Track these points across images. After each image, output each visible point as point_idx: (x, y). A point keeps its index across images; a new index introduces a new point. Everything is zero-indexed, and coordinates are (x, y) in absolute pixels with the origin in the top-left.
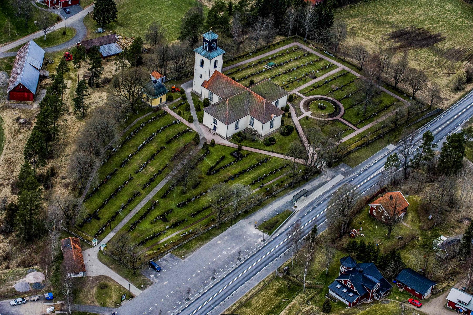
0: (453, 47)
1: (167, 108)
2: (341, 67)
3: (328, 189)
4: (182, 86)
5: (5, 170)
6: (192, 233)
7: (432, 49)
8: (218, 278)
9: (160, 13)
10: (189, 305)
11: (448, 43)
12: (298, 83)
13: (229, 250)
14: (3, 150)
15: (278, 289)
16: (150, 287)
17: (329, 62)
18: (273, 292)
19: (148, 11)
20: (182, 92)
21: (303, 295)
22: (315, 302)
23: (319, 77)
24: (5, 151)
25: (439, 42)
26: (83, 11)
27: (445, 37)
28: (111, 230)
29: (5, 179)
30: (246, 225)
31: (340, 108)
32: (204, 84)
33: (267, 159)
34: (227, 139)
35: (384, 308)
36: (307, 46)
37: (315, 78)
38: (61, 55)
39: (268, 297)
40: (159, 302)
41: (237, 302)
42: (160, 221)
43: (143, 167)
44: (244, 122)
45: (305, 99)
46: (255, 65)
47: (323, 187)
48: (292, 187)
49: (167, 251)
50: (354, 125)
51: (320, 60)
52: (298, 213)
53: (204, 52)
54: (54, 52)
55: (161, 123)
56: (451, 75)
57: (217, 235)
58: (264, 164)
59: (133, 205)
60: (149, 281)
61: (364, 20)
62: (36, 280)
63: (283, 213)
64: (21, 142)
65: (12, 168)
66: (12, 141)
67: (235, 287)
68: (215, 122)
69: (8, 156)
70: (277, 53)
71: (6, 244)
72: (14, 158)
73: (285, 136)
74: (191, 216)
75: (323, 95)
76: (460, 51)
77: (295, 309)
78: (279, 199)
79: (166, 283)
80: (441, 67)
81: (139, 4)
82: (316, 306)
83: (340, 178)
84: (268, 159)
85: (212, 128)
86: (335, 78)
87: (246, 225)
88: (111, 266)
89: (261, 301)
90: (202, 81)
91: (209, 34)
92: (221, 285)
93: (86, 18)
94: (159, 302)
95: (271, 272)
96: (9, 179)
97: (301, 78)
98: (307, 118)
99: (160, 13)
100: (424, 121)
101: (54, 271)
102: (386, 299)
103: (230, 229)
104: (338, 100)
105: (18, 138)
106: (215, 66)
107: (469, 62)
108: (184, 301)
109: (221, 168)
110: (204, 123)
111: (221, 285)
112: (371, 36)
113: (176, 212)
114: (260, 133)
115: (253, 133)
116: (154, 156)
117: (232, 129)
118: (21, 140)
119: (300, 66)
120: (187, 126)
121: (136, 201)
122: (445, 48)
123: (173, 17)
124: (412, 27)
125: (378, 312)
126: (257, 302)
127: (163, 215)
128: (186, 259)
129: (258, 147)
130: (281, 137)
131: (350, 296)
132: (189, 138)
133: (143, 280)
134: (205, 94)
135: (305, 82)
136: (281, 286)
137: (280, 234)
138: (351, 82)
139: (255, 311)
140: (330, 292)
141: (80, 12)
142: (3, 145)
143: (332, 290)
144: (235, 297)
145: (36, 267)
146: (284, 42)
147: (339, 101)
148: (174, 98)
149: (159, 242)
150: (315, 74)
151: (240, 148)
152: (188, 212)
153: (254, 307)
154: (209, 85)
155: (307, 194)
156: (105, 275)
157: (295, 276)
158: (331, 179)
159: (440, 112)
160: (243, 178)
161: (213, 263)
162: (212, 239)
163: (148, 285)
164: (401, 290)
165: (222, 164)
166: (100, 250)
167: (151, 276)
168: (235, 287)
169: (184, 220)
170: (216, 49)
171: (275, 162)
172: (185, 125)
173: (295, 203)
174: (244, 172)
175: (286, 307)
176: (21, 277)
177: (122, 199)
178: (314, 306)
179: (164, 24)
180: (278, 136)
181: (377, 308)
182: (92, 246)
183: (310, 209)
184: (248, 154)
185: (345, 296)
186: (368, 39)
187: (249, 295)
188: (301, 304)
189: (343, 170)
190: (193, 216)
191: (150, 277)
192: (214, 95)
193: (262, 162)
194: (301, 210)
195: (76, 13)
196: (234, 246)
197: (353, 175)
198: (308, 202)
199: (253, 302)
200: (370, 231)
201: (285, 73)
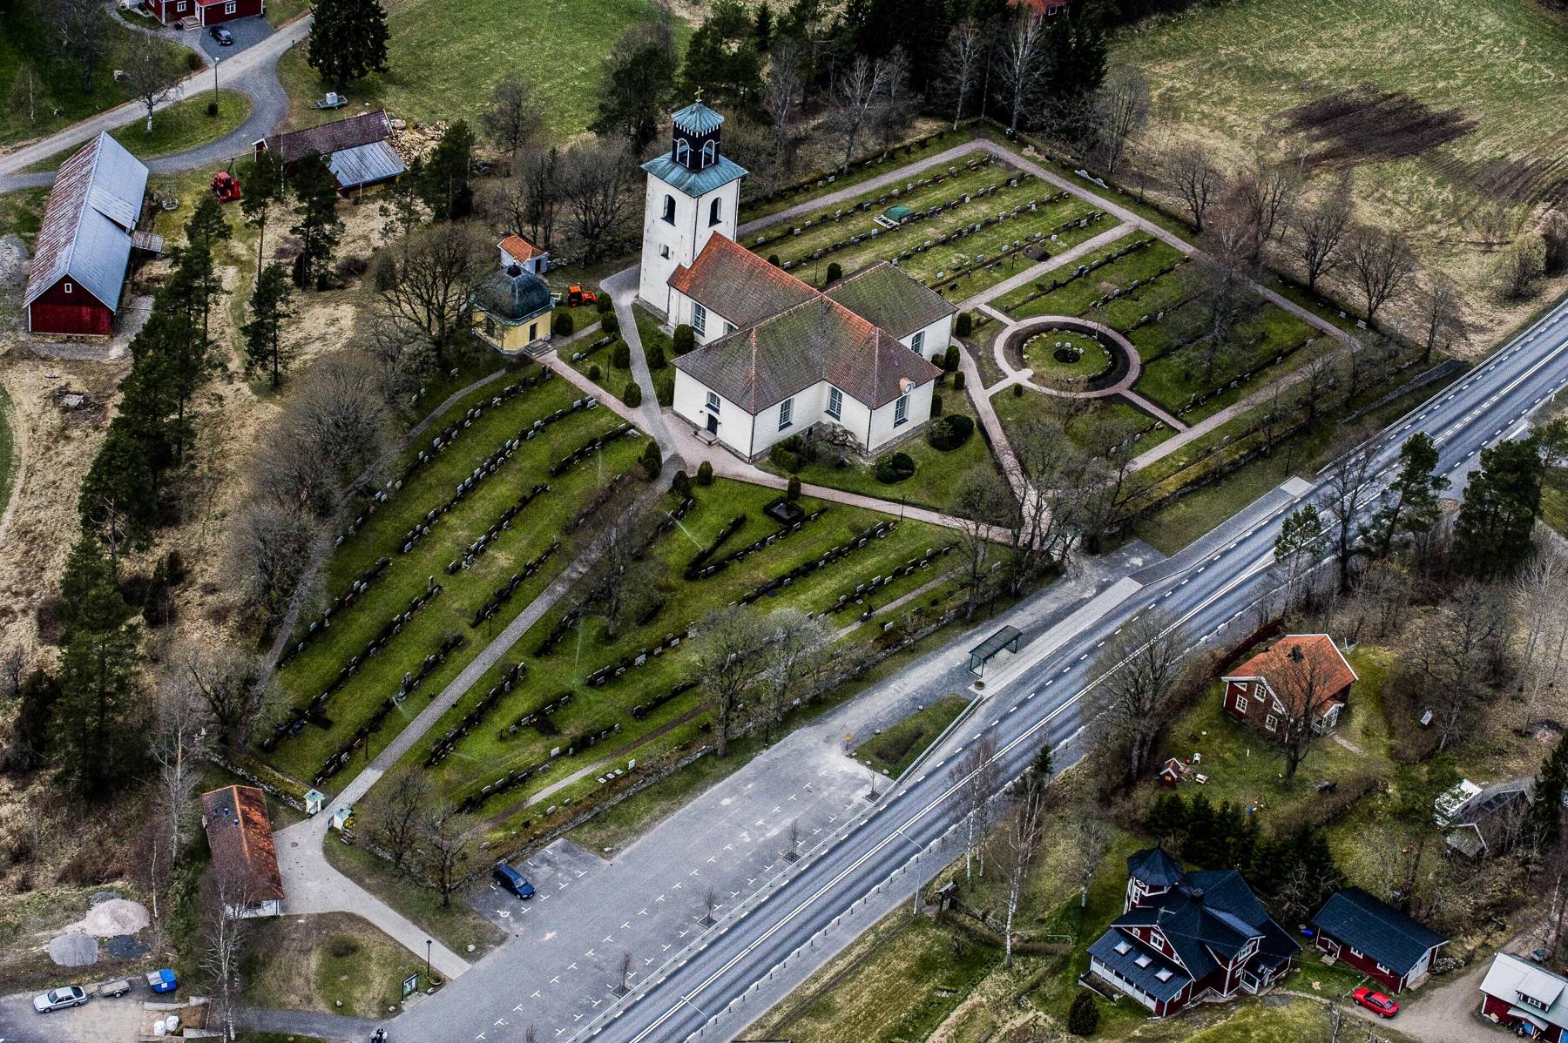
1: (552, 359)
2: (1129, 221)
3: (1086, 626)
5: (17, 564)
6: (635, 770)
8: (723, 921)
10: (627, 1011)
12: (989, 275)
14: (9, 496)
16: (497, 950)
17: (1091, 206)
18: (903, 965)
20: (605, 304)
21: (1005, 976)
22: (1044, 1001)
24: (15, 499)
25: (1456, 140)
26: (275, 37)
27: (1476, 123)
28: (368, 761)
29: (16, 594)
30: (816, 744)
31: (1126, 358)
33: (886, 527)
34: (753, 460)
35: (1275, 1020)
36: (1019, 153)
37: (1044, 257)
38: (202, 181)
39: (890, 983)
41: (787, 1000)
42: (530, 734)
43: (475, 552)
44: (809, 405)
45: (1013, 326)
46: (845, 216)
47: (1069, 619)
48: (969, 618)
49: (554, 830)
50: (1175, 415)
51: (1060, 198)
52: (988, 704)
53: (678, 172)
54: (180, 172)
55: (534, 407)
56: (1496, 248)
57: (718, 779)
58: (876, 542)
59: (440, 678)
60: (495, 930)
63: (939, 705)
64: (70, 469)
65: (40, 556)
66: (39, 465)
67: (780, 951)
68: (713, 405)
70: (917, 176)
71: (19, 807)
72: (45, 524)
74: (635, 715)
78: (927, 660)
79: (549, 936)
80: (1460, 221)
82: (1047, 1013)
83: (1126, 588)
84: (889, 526)
85: (702, 422)
86: (1110, 260)
87: (816, 744)
88: (367, 881)
89: (866, 997)
90: (669, 267)
91: (692, 113)
92: (732, 943)
93: (285, 61)
95: (900, 902)
96: (29, 593)
98: (1018, 390)
99: (529, 43)
100: (1407, 403)
101: (178, 897)
103: (763, 758)
104: (1119, 331)
105: (60, 458)
106: (714, 220)
109: (733, 556)
110: (678, 405)
111: (732, 943)
113: (582, 701)
114: (862, 439)
117: (769, 428)
118: (70, 464)
119: (994, 218)
120: (619, 418)
122: (1476, 158)
123: (575, 57)
124: (1365, 88)
125: (1253, 1034)
126: (851, 1001)
127: (539, 712)
128: (617, 859)
129: (856, 487)
130: (933, 453)
132: (628, 455)
133: (474, 927)
134: (680, 310)
135: (1012, 272)
137: (929, 776)
138: (1163, 272)
140: (1095, 967)
142: (9, 480)
143: (1100, 961)
146: (942, 140)
147: (1126, 334)
150: (1044, 244)
151: (794, 489)
153: (843, 1015)
155: (1016, 642)
156: (348, 909)
157: (979, 913)
158: (1096, 595)
159: (1457, 370)
161: (707, 870)
162: (702, 790)
164: (1329, 961)
165: (738, 542)
166: (332, 829)
167: (501, 913)
168: (780, 951)
169: (611, 729)
171: (911, 535)
172: (613, 413)
173: (978, 671)
175: (947, 1016)
176: (68, 917)
177: (405, 660)
178: (1040, 1013)
180: (920, 451)
181: (1251, 1019)
182: (305, 816)
183: (1028, 692)
184: (822, 511)
185: (1143, 980)
186: (1221, 129)
187: (826, 978)
188: (996, 1006)
189: (1138, 561)
190: (641, 714)
191: (497, 917)
193: (869, 535)
194: (998, 694)
196: (776, 815)
197: (1170, 580)
198: (1023, 670)
199: (839, 1000)
200: (1224, 762)
201: (944, 243)
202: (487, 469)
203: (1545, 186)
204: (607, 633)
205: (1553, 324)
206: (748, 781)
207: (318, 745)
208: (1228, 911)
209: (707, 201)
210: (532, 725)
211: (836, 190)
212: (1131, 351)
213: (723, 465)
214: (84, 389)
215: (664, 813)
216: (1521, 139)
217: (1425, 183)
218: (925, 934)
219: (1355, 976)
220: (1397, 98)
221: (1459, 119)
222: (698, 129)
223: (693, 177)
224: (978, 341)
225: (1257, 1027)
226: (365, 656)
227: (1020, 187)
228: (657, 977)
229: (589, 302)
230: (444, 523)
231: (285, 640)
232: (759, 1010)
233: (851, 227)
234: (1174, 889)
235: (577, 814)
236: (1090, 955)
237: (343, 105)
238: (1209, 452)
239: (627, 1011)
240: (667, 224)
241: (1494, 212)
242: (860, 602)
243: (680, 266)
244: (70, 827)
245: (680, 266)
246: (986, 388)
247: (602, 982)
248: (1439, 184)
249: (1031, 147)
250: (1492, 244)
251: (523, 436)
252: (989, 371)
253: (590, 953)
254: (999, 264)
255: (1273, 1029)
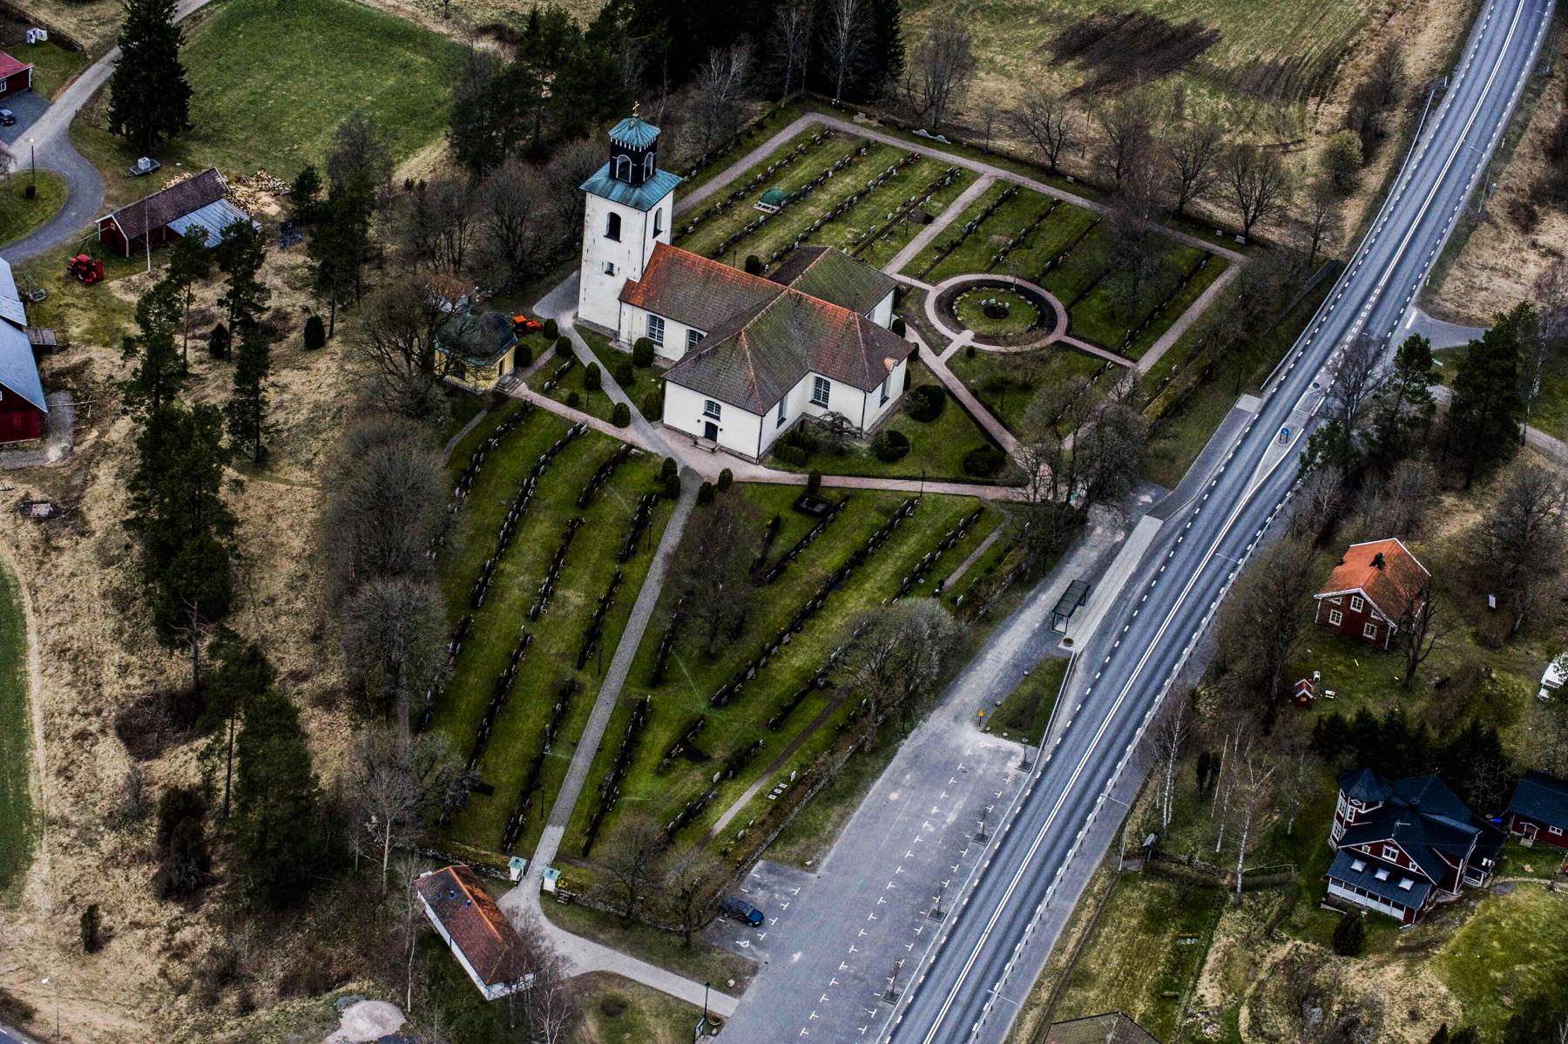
0: (1256, 60)
1: (523, 391)
2: (986, 176)
3: (1133, 568)
4: (541, 310)
5: (71, 684)
6: (800, 781)
7: (1197, 73)
8: (951, 910)
9: (305, 80)
10: (905, 1014)
11: (1234, 48)
12: (888, 245)
13: (936, 816)
14: (23, 617)
15: (1146, 909)
16: (755, 980)
17: (949, 165)
18: (1134, 922)
19: (258, 79)
20: (550, 329)
21: (1239, 914)
22: (1296, 931)
23: (938, 215)
24: (32, 620)
25: (1208, 50)
26: (53, 110)
27: (1218, 31)
28: (545, 819)
29: (86, 715)
30: (948, 725)
31: (1050, 306)
32: (628, 295)
33: (911, 503)
34: (760, 460)
35: (1513, 908)
36: (851, 121)
37: (928, 220)
38: (55, 266)
39: (1131, 941)
40: (809, 1025)
41: (1044, 975)
42: (683, 764)
43: (545, 594)
44: (798, 400)
45: (933, 293)
46: (726, 208)
47: (1114, 565)
48: (1028, 579)
49: (753, 853)
50: (1118, 353)
51: (912, 161)
52: (1083, 659)
53: (619, 189)
54: (30, 261)
55: (530, 443)
56: (1292, 147)
57: (875, 775)
58: (908, 520)
59: (576, 721)
60: (744, 961)
61: (952, 11)
62: (379, 1028)
63: (1040, 668)
64: (76, 580)
65: (90, 673)
66: (39, 581)
67: (1013, 931)
68: (712, 410)
69: (53, 636)
70: (769, 159)
71: (199, 929)
72: (78, 639)
73: (932, 420)
74: (771, 728)
75: (981, 272)
76: (1282, 69)
77: (1238, 962)
78: (1008, 627)
79: (797, 957)
80: (1248, 126)
81: (221, 61)
82: (1306, 941)
83: (1148, 528)
84: (913, 502)
85: (700, 431)
86: (988, 213)
87: (948, 725)
88: (601, 936)
89: (1115, 959)
90: (618, 282)
91: (630, 128)
92: (967, 932)
93: (78, 130)
94: (809, 1025)
95: (1097, 863)
96: (99, 712)
97: (888, 227)
98: (971, 353)
99: (305, 80)
100: (1306, 306)
101: (424, 988)
102: (1501, 879)
103: (907, 747)
104: (1031, 281)
105: (60, 571)
106: (657, 232)
107: (1322, 99)
108: (881, 1004)
109: (786, 557)
110: (668, 418)
111: (967, 932)
112: (999, 58)
113: (716, 723)
114: (857, 424)
115: (838, 424)
116: (562, 553)
117: (771, 428)
118: (73, 575)
119: (864, 188)
120: (615, 440)
121: (579, 711)
122: (1233, 65)
123: (357, 87)
124: (1104, 11)
125: (1503, 924)
126: (1104, 964)
127: (683, 741)
128: (821, 871)
129: (865, 471)
130: (920, 427)
131: (1405, 890)
132: (638, 478)
133: (723, 962)
134: (633, 325)
135: (906, 239)
136: (1151, 901)
137: (1065, 736)
138: (1041, 218)
139: (1114, 992)
140: (1333, 889)
141: (44, 111)
142: (15, 601)
143: (1338, 882)
144: (1028, 959)
145: (353, 986)
146: (778, 119)
147: (1037, 283)
148: (535, 351)
149: (711, 830)
150: (922, 206)
151: (814, 482)
152: (754, 719)
153: (1103, 979)
154: (645, 293)
155: (1080, 594)
156: (594, 968)
157: (1184, 858)
158: (1127, 537)
159: (1335, 270)
160: (867, 577)
161: (909, 865)
162: (867, 789)
163: (745, 974)
164: (1528, 843)
165: (782, 543)
166: (543, 892)
167: (742, 944)
168: (1013, 931)
169: (756, 744)
170: (654, 173)
171: (936, 509)
172: (606, 436)
173: (1060, 627)
174: (859, 560)
175: (1203, 962)
176: (324, 1028)
177: (532, 715)
178: (1298, 942)
179: (337, 113)
180: (903, 423)
181: (1493, 910)
182: (511, 885)
183: (1111, 641)
184: (846, 499)
185: (1388, 892)
186: (994, 70)
187: (1070, 947)
188: (1248, 943)
189: (1147, 499)
190: (777, 726)
191: (738, 948)
192: (669, 324)
193: (900, 515)
194: (1088, 647)
195: (35, 119)
196: (946, 800)
197: (1183, 512)
198: (1099, 620)
199: (1093, 966)
200: (1341, 675)
201: (831, 220)
202: (518, 510)
203: (1305, 82)
204: (708, 652)
205: (1391, 213)
206: (903, 773)
207: (490, 811)
208: (1441, 814)
209: (651, 214)
210: (681, 754)
211: (703, 182)
212: (1050, 297)
213: (743, 472)
214: (46, 496)
215: (844, 817)
216: (1264, 40)
217: (1199, 95)
218: (1140, 888)
219: (1557, 853)
220: (1137, 18)
221: (1201, 30)
222: (641, 143)
223: (637, 192)
224: (909, 310)
225: (1503, 917)
226: (491, 714)
227: (870, 154)
228: (917, 977)
229: (534, 329)
230: (502, 571)
231: (407, 713)
232: (1023, 992)
233: (736, 217)
234: (1387, 803)
235: (767, 834)
236: (1328, 878)
237: (158, 169)
238: (1165, 384)
239: (905, 1014)
240: (611, 242)
241: (1273, 113)
242: (922, 581)
243: (628, 281)
244: (265, 940)
245: (628, 281)
246: (938, 354)
247: (869, 990)
248: (1212, 94)
249: (861, 114)
250: (1286, 145)
251: (535, 472)
252: (934, 340)
253: (843, 966)
254: (891, 234)
255: (1516, 916)
